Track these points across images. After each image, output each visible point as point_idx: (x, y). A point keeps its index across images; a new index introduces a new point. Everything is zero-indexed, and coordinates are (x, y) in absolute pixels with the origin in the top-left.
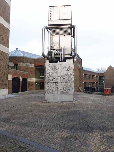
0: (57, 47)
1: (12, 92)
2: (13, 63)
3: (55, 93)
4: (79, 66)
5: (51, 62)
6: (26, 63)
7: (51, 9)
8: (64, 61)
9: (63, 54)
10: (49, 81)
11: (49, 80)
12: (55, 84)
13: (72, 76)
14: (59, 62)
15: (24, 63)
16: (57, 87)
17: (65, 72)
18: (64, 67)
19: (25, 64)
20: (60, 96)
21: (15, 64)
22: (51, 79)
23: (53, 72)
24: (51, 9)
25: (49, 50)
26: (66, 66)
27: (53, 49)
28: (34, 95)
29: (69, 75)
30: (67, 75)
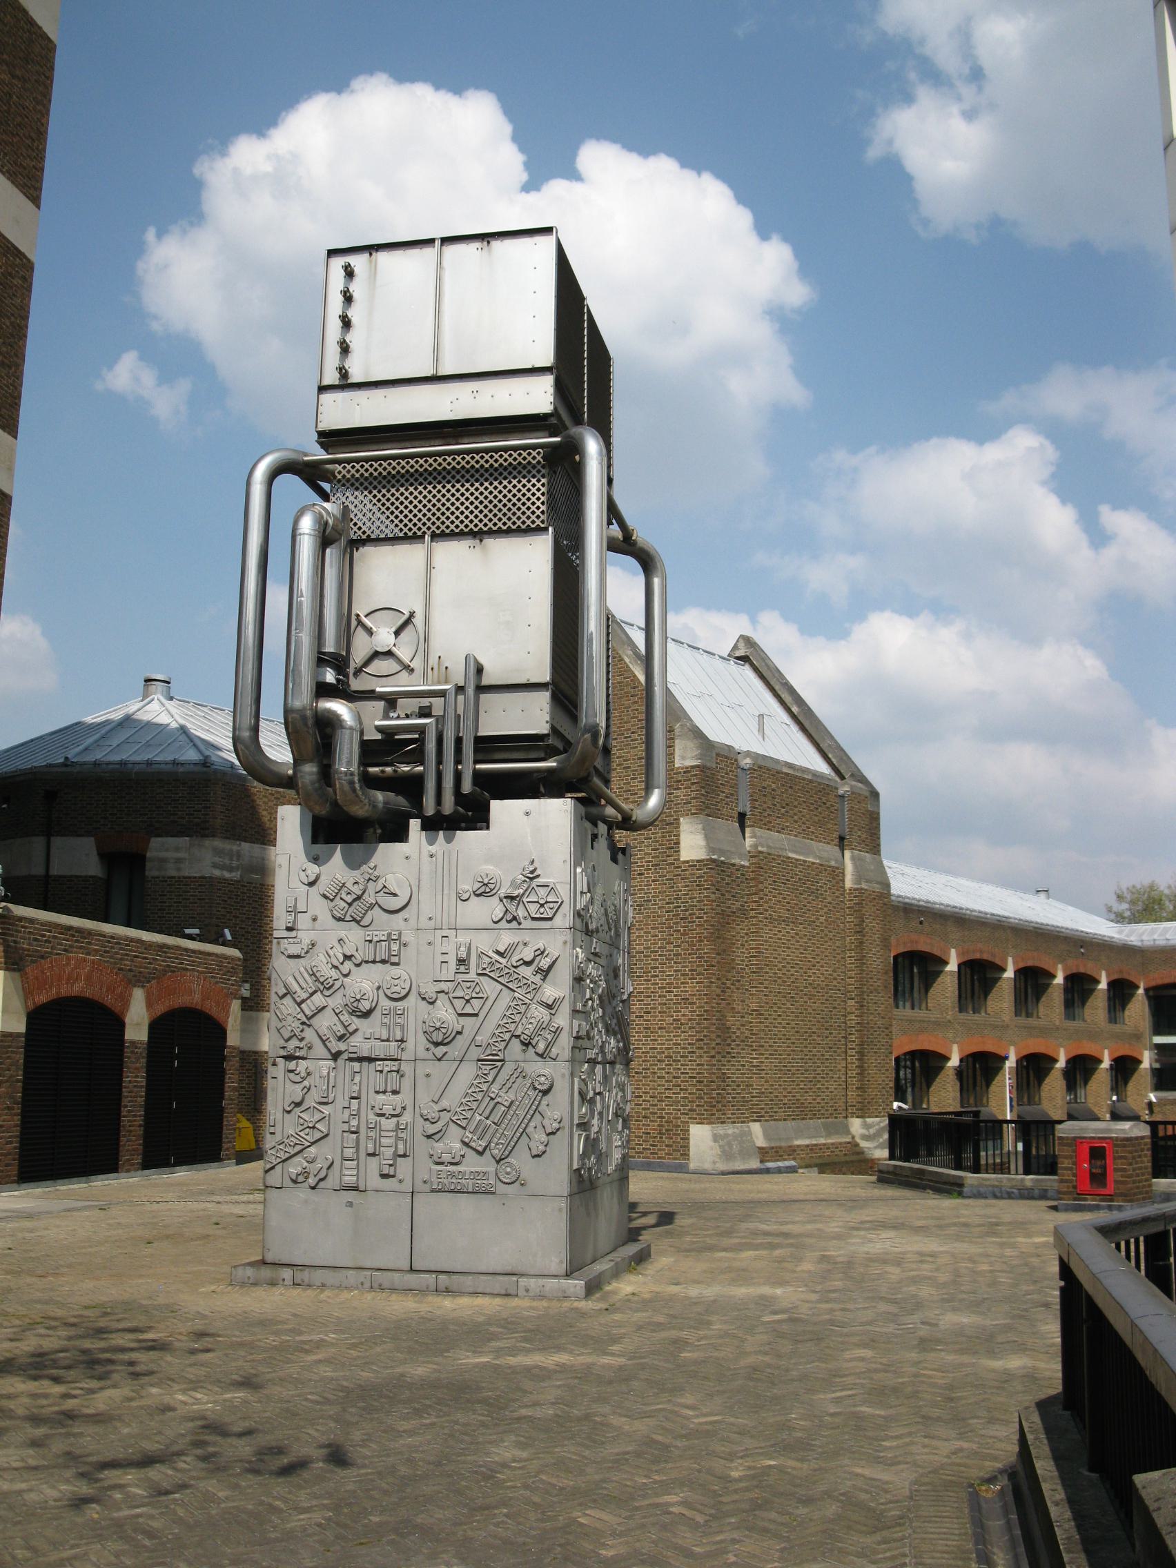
0: (395, 667)
1: (14, 1171)
2: (92, 839)
3: (374, 1181)
4: (837, 874)
5: (335, 829)
6: (233, 846)
7: (349, 273)
8: (473, 815)
11: (309, 1034)
12: (370, 1077)
13: (557, 988)
14: (415, 824)
15: (208, 842)
16: (388, 1109)
17: (484, 943)
18: (467, 886)
19: (218, 852)
21: (107, 857)
22: (325, 1023)
23: (354, 937)
24: (349, 273)
25: (303, 698)
26: (490, 869)
27: (356, 684)
28: (238, 1210)
29: (526, 971)
30: (503, 969)
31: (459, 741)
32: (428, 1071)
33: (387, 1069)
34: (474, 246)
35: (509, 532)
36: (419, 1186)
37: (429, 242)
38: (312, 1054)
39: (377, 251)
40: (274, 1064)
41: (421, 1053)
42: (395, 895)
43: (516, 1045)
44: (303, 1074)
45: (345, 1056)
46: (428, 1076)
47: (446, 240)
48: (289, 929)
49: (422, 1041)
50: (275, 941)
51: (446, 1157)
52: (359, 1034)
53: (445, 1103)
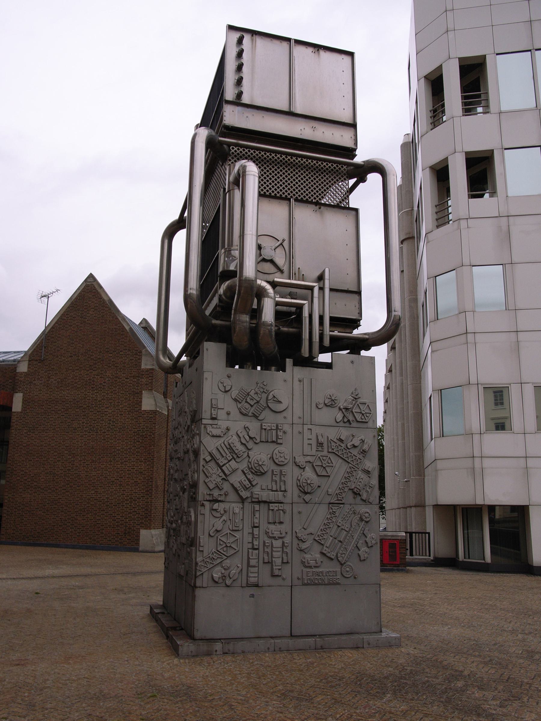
10: (226, 495)
11: (226, 487)
17: (333, 434)
18: (319, 398)
23: (254, 426)
29: (355, 452)
31: (321, 318)
32: (300, 510)
33: (276, 508)
34: (310, 50)
35: (275, 197)
36: (296, 582)
37: (288, 40)
38: (229, 498)
39: (256, 34)
40: (203, 505)
41: (296, 499)
42: (280, 402)
43: (350, 495)
44: (222, 512)
45: (249, 500)
46: (300, 513)
47: (299, 42)
48: (213, 419)
49: (296, 492)
50: (203, 426)
51: (312, 563)
52: (258, 486)
53: (310, 530)
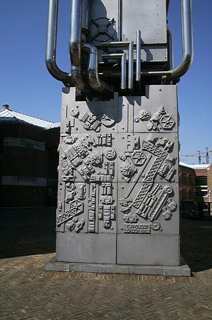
3: (102, 229)
8: (138, 91)
9: (135, 64)
14: (116, 94)
20: (123, 238)
23: (93, 135)
41: (120, 179)
